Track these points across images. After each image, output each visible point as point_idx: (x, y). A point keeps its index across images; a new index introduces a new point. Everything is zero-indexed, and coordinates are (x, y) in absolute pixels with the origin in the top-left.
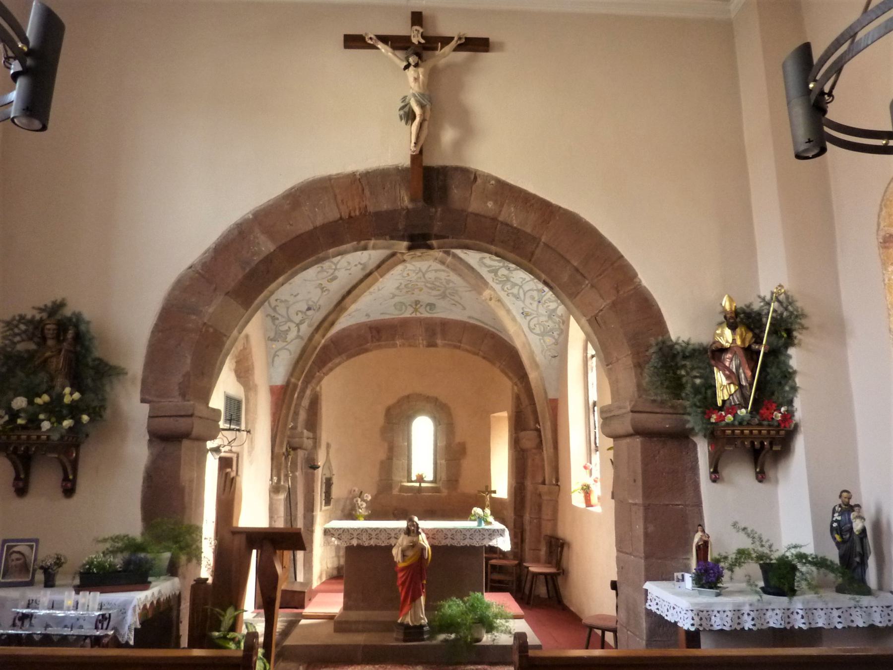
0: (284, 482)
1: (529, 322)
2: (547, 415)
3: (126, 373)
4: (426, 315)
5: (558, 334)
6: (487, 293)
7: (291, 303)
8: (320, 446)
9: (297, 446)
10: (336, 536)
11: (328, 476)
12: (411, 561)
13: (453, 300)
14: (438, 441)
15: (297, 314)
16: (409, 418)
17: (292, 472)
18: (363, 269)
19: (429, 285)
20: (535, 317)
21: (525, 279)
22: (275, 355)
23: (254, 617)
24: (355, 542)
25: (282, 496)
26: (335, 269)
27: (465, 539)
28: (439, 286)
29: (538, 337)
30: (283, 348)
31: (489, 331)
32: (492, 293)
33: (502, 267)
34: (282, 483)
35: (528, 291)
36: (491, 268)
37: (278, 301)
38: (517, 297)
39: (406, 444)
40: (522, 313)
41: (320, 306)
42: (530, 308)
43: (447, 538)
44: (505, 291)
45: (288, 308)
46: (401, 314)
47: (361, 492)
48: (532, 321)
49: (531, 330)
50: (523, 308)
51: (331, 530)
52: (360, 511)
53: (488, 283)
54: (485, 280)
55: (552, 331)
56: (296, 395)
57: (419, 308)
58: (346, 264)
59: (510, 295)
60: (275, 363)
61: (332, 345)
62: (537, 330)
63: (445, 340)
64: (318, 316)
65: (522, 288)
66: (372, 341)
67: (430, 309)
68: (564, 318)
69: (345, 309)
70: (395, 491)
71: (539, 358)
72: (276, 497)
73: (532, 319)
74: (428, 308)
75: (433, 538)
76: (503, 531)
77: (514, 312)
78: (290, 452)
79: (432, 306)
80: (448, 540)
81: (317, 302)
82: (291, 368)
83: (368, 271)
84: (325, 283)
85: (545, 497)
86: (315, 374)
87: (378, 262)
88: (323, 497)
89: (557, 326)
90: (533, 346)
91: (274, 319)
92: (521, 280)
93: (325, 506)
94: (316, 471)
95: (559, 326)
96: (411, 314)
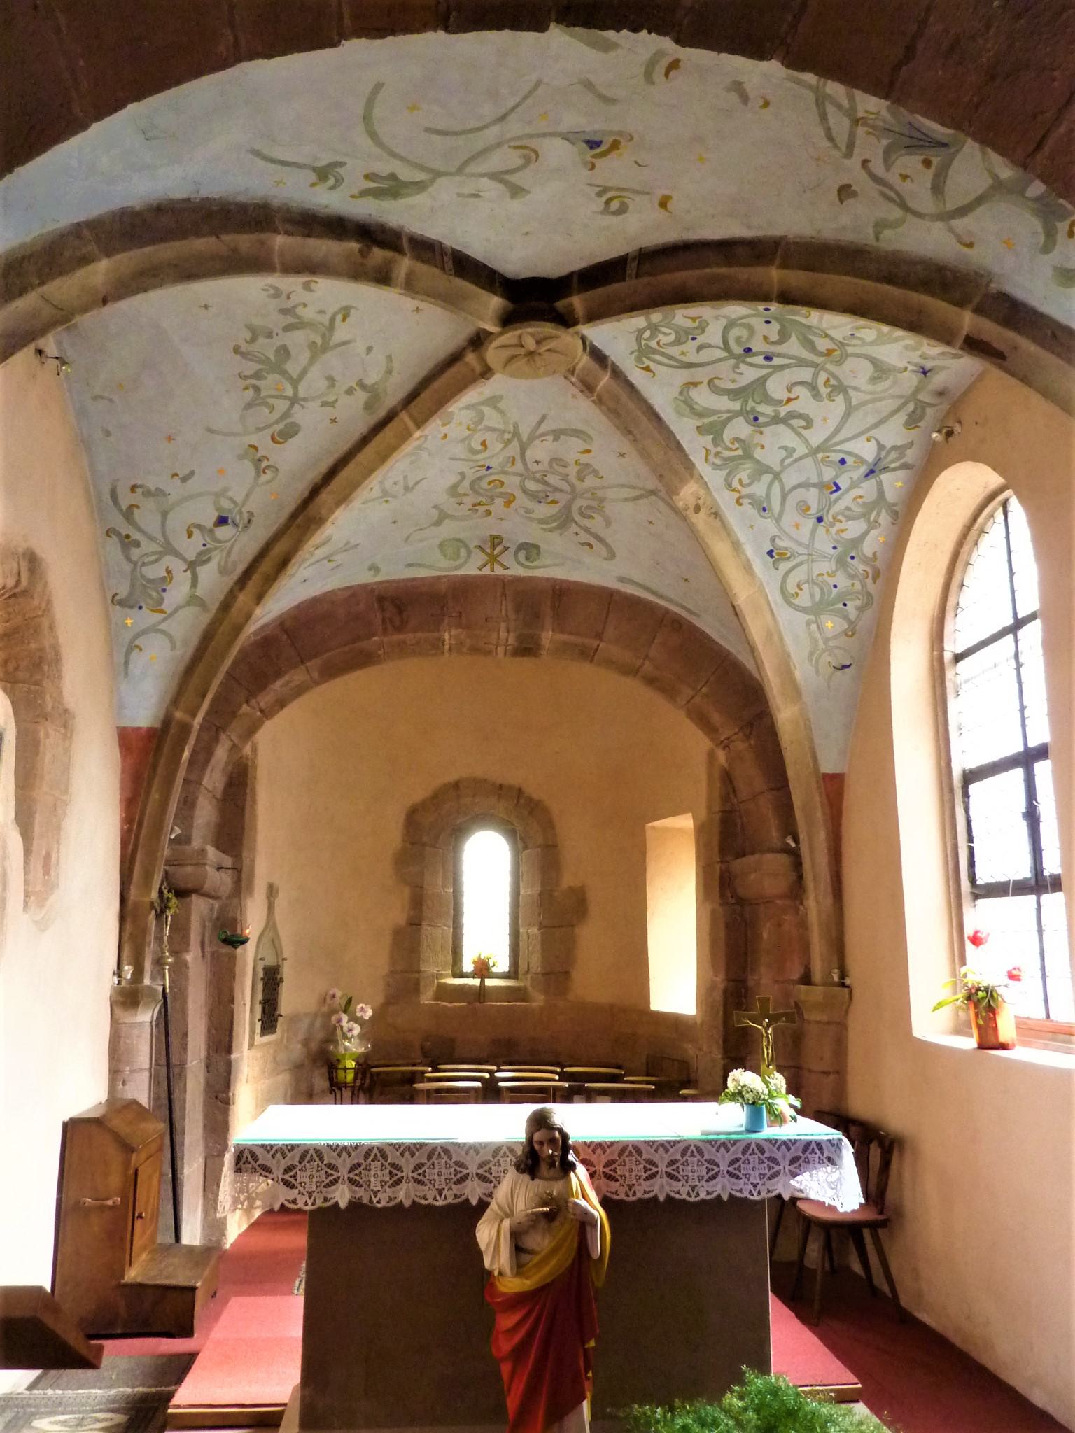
0: (153, 978)
1: (787, 573)
2: (819, 814)
3: (452, 1040)
4: (517, 571)
7: (172, 499)
8: (250, 889)
9: (190, 886)
10: (278, 1173)
11: (271, 961)
12: (546, 1270)
13: (587, 530)
15: (190, 535)
16: (458, 833)
17: (175, 953)
18: (368, 406)
19: (532, 486)
20: (801, 563)
21: (794, 450)
22: (132, 647)
23: (31, 1387)
24: (342, 1196)
25: (146, 1016)
26: (294, 400)
27: (713, 1177)
28: (556, 489)
30: (153, 629)
31: (667, 611)
32: (702, 492)
33: (737, 414)
34: (147, 981)
35: (795, 488)
36: (706, 421)
37: (139, 491)
40: (770, 553)
41: (251, 514)
42: (792, 539)
43: (654, 1175)
44: (734, 490)
45: (164, 514)
46: (456, 568)
47: (350, 1000)
49: (787, 597)
50: (773, 540)
51: (258, 1152)
52: (347, 1044)
53: (693, 465)
54: (686, 456)
56: (186, 754)
57: (501, 553)
58: (323, 384)
59: (746, 501)
60: (131, 667)
62: (804, 600)
63: (562, 632)
64: (244, 545)
65: (781, 481)
66: (385, 631)
67: (527, 559)
68: (878, 564)
69: (319, 522)
70: (426, 998)
71: (803, 672)
72: (128, 1018)
73: (793, 568)
74: (522, 555)
75: (609, 1177)
76: (836, 1145)
77: (749, 551)
78: (168, 899)
79: (530, 550)
80: (658, 1181)
81: (244, 504)
82: (174, 684)
83: (381, 413)
84: (262, 441)
85: (812, 1016)
86: (240, 706)
87: (409, 387)
88: (258, 1015)
89: (858, 586)
90: (788, 641)
91: (127, 543)
92: (784, 454)
93: (263, 1034)
94: (239, 950)
95: (863, 585)
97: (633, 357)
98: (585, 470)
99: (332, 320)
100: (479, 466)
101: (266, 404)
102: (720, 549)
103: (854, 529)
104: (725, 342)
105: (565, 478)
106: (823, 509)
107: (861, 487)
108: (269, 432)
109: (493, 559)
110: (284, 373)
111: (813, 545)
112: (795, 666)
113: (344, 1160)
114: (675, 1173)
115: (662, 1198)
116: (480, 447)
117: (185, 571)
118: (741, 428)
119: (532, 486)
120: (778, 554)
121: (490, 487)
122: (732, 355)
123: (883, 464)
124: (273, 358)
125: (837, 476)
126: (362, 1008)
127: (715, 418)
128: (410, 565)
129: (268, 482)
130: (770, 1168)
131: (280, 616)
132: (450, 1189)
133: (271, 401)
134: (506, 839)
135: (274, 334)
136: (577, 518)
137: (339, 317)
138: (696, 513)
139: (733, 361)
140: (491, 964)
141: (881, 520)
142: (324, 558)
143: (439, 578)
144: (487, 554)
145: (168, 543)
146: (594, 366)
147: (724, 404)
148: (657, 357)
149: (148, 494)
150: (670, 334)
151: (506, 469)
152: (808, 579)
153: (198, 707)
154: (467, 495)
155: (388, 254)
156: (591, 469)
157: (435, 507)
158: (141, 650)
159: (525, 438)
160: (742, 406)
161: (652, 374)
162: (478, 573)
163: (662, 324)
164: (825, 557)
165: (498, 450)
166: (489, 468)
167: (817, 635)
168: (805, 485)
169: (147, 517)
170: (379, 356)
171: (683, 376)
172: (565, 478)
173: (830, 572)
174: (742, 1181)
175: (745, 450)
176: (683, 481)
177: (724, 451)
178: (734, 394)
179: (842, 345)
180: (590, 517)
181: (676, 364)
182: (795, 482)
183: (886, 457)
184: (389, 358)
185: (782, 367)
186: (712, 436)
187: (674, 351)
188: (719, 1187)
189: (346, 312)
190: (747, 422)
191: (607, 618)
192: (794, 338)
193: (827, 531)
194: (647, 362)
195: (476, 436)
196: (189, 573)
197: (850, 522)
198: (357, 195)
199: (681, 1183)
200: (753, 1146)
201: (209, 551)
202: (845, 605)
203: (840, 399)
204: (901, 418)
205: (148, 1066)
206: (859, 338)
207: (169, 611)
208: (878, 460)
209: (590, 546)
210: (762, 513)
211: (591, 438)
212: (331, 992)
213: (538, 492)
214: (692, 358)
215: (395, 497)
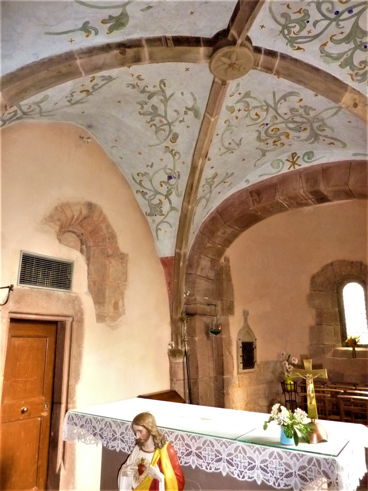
4: (305, 165)
7: (151, 174)
15: (162, 186)
25: (180, 360)
28: (302, 123)
30: (162, 222)
32: (356, 96)
34: (180, 348)
36: (342, 60)
37: (140, 175)
45: (151, 181)
46: (279, 171)
47: (289, 356)
53: (347, 85)
58: (175, 114)
60: (159, 236)
67: (308, 159)
74: (306, 158)
86: (206, 244)
96: (289, 169)
97: (288, 46)
98: (307, 109)
99: (161, 87)
101: (161, 129)
104: (323, 15)
105: (301, 116)
109: (294, 163)
110: (160, 115)
116: (256, 117)
117: (165, 199)
119: (291, 126)
124: (152, 111)
126: (294, 359)
127: (345, 57)
129: (179, 159)
131: (216, 208)
133: (162, 127)
134: (361, 285)
135: (147, 102)
136: (319, 132)
137: (163, 86)
138: (355, 107)
139: (334, 23)
140: (357, 341)
143: (272, 178)
144: (291, 162)
145: (156, 191)
146: (269, 58)
147: (345, 47)
148: (299, 40)
149: (143, 175)
150: (295, 26)
151: (275, 122)
154: (268, 139)
155: (136, 49)
156: (308, 108)
158: (160, 230)
159: (273, 106)
160: (354, 44)
161: (303, 50)
162: (289, 171)
163: (287, 23)
165: (265, 115)
166: (267, 124)
169: (146, 183)
170: (187, 95)
172: (301, 116)
177: (359, 72)
178: (347, 39)
180: (324, 130)
186: (349, 66)
187: (304, 33)
191: (349, 175)
194: (297, 45)
195: (251, 113)
196: (167, 199)
199: (234, 468)
201: (170, 190)
205: (182, 378)
207: (165, 214)
209: (333, 144)
211: (298, 93)
212: (282, 353)
213: (295, 127)
214: (315, 32)
215: (234, 149)
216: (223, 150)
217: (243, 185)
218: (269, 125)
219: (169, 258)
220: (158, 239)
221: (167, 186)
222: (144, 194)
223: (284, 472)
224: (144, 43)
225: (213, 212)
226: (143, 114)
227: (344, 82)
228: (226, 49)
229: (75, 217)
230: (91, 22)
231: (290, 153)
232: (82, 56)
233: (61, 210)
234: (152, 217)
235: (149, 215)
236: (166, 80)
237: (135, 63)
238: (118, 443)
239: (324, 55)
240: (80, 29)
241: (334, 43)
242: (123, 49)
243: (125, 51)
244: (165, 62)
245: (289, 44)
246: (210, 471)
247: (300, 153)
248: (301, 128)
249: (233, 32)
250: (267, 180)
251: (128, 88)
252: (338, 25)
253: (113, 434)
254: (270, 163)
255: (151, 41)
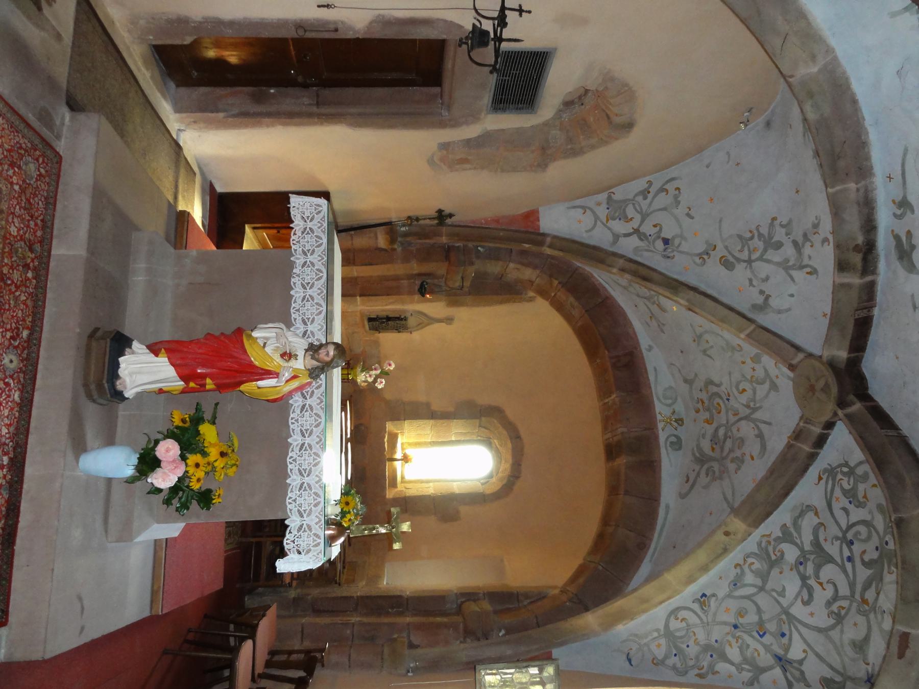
5: (674, 665)
6: (737, 525)
7: (676, 211)
14: (459, 483)
15: (655, 226)
19: (721, 432)
21: (784, 596)
25: (382, 241)
26: (749, 262)
27: (301, 474)
29: (662, 628)
30: (597, 218)
31: (651, 540)
32: (739, 536)
33: (802, 549)
36: (792, 530)
37: (677, 192)
38: (735, 584)
39: (453, 439)
40: (704, 595)
43: (303, 435)
44: (745, 560)
45: (665, 209)
46: (658, 399)
48: (691, 613)
49: (674, 612)
50: (714, 595)
55: (679, 653)
58: (763, 276)
60: (573, 210)
61: (600, 300)
62: (674, 625)
64: (654, 259)
67: (672, 443)
70: (390, 426)
71: (622, 629)
74: (673, 439)
77: (704, 579)
80: (302, 223)
86: (556, 279)
89: (691, 663)
90: (644, 617)
92: (780, 589)
95: (693, 667)
98: (740, 461)
100: (728, 393)
101: (743, 247)
102: (701, 556)
103: (733, 653)
105: (731, 451)
106: (743, 627)
107: (766, 654)
108: (727, 254)
110: (765, 251)
111: (717, 624)
112: (626, 624)
113: (317, 225)
114: (304, 448)
115: (288, 481)
116: (741, 389)
117: (633, 228)
118: (791, 553)
119: (721, 432)
120: (704, 601)
121: (716, 405)
122: (845, 532)
123: (788, 667)
124: (773, 241)
125: (771, 634)
127: (795, 534)
128: (655, 370)
129: (695, 263)
130: (305, 531)
131: (612, 297)
132: (295, 507)
133: (746, 249)
135: (789, 236)
136: (705, 467)
137: (808, 270)
139: (840, 535)
141: (744, 673)
142: (652, 314)
143: (650, 388)
145: (648, 215)
146: (813, 439)
147: (807, 538)
148: (830, 482)
149: (676, 197)
150: (849, 485)
152: (689, 626)
153: (555, 249)
155: (859, 265)
157: (696, 375)
158: (584, 213)
159: (753, 416)
163: (856, 476)
164: (708, 635)
166: (728, 400)
167: (650, 638)
168: (759, 611)
169: (663, 200)
171: (820, 503)
172: (731, 451)
173: (698, 641)
174: (298, 492)
175: (776, 560)
176: (744, 519)
177: (772, 546)
178: (816, 544)
179: (874, 609)
180: (707, 475)
181: (828, 498)
182: (760, 603)
183: (794, 667)
184: (789, 310)
185: (845, 571)
186: (781, 535)
187: (838, 493)
188: (297, 289)
189: (814, 272)
190: (798, 557)
192: (869, 572)
193: (728, 633)
194: (825, 477)
196: (632, 231)
197: (738, 649)
198: (894, 234)
199: (298, 452)
200: (319, 459)
201: (647, 239)
202: (675, 655)
203: (832, 621)
204: (828, 673)
206: (883, 618)
208: (790, 662)
209: (687, 481)
210: (733, 583)
214: (836, 506)
215: (698, 344)
216: (699, 330)
217: (644, 340)
218: (726, 402)
219: (537, 223)
220: (569, 208)
221: (654, 234)
222: (645, 193)
223: (303, 509)
224: (869, 278)
225: (606, 290)
226: (772, 225)
227: (763, 525)
228: (834, 390)
229: (610, 107)
230: (912, 216)
231: (684, 417)
232: (862, 191)
233: (622, 91)
234: (605, 202)
235: (609, 198)
236: (817, 278)
237: (837, 264)
238: (300, 292)
239: (804, 508)
240: (905, 197)
241: (815, 526)
242: (863, 250)
243: (859, 252)
244: (833, 302)
245: (829, 467)
246: (290, 423)
247: (681, 432)
248: (716, 444)
249: (857, 407)
250: (649, 380)
251: (815, 218)
252: (837, 538)
253: (309, 283)
254: (673, 385)
255: (869, 291)
